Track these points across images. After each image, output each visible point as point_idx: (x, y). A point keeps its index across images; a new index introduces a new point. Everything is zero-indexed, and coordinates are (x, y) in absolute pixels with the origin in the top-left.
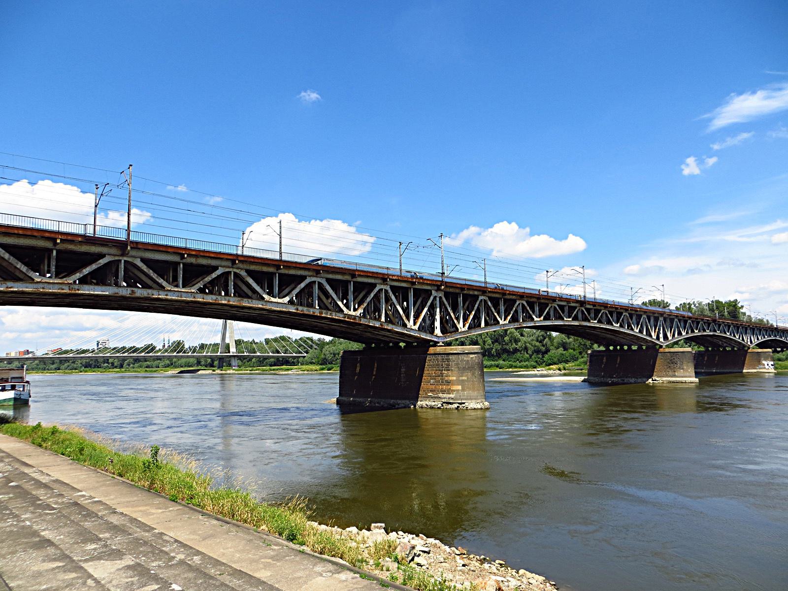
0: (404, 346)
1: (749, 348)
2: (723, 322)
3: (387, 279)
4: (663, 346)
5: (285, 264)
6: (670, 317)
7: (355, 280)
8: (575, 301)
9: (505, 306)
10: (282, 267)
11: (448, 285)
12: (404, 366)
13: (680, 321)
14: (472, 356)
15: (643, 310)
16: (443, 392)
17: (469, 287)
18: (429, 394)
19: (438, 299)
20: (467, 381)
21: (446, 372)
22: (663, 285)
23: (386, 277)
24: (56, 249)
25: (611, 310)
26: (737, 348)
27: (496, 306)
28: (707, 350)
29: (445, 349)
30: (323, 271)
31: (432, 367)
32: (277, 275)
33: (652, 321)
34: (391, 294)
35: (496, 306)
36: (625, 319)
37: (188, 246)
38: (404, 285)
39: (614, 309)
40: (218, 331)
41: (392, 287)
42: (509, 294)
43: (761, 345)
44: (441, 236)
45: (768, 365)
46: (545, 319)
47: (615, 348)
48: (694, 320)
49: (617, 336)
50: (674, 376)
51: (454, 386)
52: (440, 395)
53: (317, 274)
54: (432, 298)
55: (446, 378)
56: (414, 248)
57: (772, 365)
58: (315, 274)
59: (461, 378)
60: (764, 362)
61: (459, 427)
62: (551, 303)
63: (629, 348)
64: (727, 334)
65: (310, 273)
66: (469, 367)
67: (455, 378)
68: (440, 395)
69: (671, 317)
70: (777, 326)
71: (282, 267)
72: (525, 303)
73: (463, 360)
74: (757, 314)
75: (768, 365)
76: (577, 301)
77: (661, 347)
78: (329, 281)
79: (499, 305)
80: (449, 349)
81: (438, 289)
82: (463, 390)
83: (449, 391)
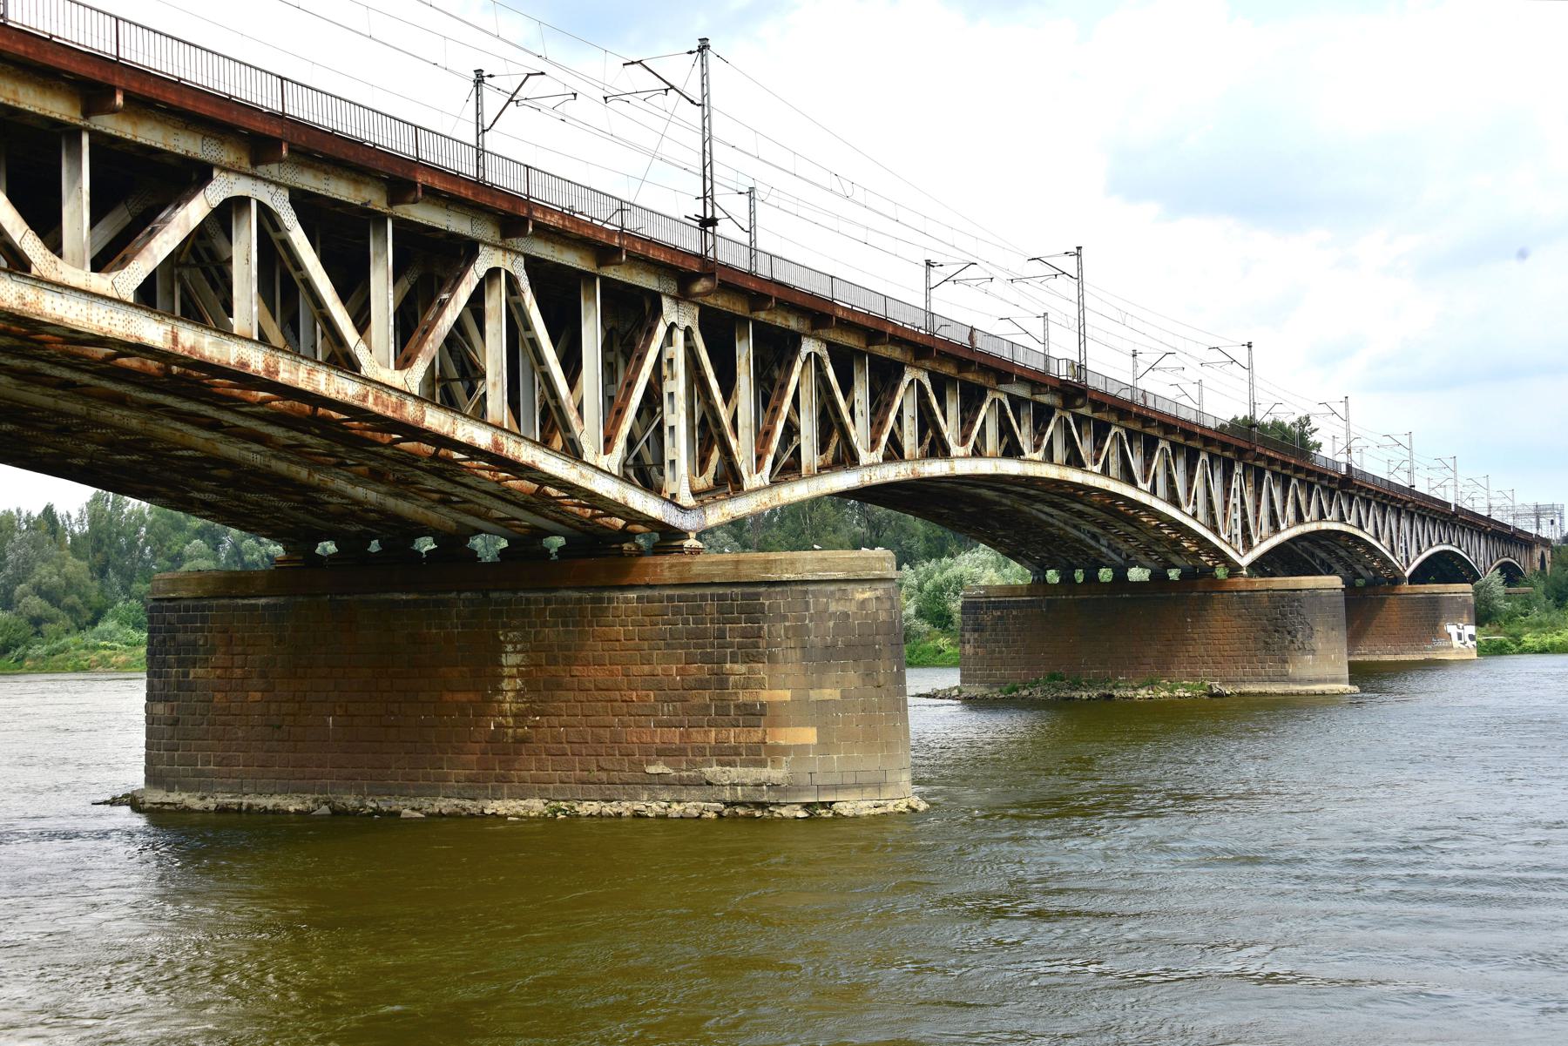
3: (525, 221)
5: (135, 87)
9: (406, 285)
10: (119, 100)
11: (733, 282)
12: (515, 644)
13: (844, 361)
16: (726, 755)
18: (652, 770)
19: (679, 336)
20: (843, 704)
21: (740, 668)
22: (1249, 346)
23: (524, 212)
28: (1040, 581)
29: (737, 562)
31: (668, 646)
33: (744, 353)
36: (496, 304)
47: (1067, 579)
50: (1284, 678)
52: (712, 771)
53: (255, 163)
55: (743, 696)
57: (1472, 637)
59: (815, 695)
60: (1452, 629)
63: (1120, 575)
64: (1141, 485)
66: (848, 646)
67: (786, 695)
68: (712, 771)
70: (1349, 467)
71: (119, 100)
73: (822, 615)
78: (303, 203)
80: (753, 564)
81: (683, 296)
82: (825, 745)
83: (757, 755)
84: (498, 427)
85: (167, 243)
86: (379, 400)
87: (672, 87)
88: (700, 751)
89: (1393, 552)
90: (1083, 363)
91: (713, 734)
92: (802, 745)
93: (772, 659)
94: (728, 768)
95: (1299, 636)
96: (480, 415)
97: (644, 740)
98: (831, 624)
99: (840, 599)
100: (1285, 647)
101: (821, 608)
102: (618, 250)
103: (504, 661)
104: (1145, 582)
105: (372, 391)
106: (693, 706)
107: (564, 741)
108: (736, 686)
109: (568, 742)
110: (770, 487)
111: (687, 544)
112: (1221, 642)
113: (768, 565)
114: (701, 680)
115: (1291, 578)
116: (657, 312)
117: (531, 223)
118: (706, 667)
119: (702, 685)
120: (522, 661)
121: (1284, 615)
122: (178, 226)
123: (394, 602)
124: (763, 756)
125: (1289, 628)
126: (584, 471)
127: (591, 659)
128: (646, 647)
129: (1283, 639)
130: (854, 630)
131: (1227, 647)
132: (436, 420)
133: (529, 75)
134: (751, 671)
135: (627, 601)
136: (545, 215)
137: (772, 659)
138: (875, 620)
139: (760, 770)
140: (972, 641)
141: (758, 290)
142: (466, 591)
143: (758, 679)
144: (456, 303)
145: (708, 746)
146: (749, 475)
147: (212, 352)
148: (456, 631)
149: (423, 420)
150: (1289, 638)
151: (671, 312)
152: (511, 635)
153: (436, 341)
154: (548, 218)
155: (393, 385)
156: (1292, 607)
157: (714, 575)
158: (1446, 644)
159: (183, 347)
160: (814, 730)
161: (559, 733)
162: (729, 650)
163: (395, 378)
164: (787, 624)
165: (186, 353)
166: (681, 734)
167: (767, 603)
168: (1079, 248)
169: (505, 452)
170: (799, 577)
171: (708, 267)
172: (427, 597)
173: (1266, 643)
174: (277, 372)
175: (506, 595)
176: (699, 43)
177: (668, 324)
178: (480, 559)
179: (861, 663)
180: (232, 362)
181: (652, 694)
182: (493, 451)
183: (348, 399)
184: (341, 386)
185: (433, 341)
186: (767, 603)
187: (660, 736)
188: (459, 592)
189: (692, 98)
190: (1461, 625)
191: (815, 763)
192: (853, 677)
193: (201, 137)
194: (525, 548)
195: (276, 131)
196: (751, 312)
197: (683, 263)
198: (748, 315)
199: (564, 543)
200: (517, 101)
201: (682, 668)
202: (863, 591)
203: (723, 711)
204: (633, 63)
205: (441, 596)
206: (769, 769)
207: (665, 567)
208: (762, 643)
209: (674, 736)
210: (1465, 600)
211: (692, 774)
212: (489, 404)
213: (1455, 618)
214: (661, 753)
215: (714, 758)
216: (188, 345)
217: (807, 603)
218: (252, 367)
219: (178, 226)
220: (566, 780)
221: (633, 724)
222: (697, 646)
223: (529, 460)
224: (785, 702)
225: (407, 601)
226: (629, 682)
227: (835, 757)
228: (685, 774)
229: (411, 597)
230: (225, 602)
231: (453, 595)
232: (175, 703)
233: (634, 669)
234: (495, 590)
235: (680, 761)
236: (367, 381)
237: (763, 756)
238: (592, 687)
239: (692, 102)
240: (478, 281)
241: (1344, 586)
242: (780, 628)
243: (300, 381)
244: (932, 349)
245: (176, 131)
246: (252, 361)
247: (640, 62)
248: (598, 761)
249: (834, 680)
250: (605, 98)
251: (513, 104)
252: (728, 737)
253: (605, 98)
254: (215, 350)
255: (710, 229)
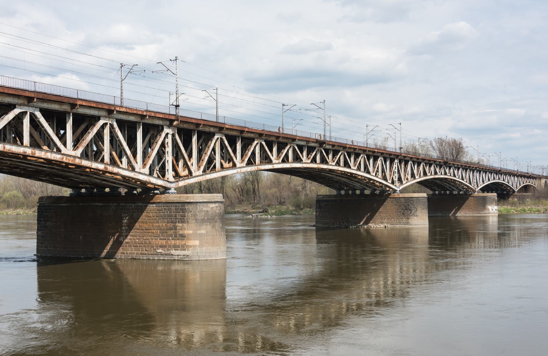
0: (126, 193)
1: (474, 191)
2: (454, 164)
3: (113, 111)
4: (397, 191)
6: (430, 162)
7: (74, 111)
8: (315, 141)
11: (185, 121)
14: (213, 205)
15: (380, 151)
16: (176, 247)
17: (206, 123)
18: (158, 251)
21: (180, 225)
23: (113, 108)
24: (197, 130)
25: (349, 150)
26: (86, 188)
27: (233, 145)
29: (180, 197)
30: (37, 98)
31: (163, 219)
32: (141, 123)
34: (117, 130)
35: (233, 145)
36: (107, 131)
37: (337, 141)
38: (132, 118)
39: (352, 150)
40: (25, 181)
41: (119, 122)
42: (248, 132)
43: (487, 189)
44: (176, 59)
45: (492, 210)
46: (283, 161)
48: (427, 162)
49: (352, 180)
51: (190, 241)
53: (29, 102)
54: (163, 135)
55: (181, 232)
56: (140, 72)
58: (26, 103)
59: (198, 232)
61: (295, 269)
62: (291, 143)
65: (20, 101)
67: (191, 232)
69: (406, 159)
72: (264, 143)
73: (201, 211)
74: (482, 154)
75: (492, 210)
76: (317, 141)
77: (395, 191)
79: (420, 165)
80: (184, 198)
81: (170, 125)
82: (201, 245)
83: (184, 247)
84: (107, 164)
85: (2, 124)
86: (67, 159)
87: (169, 70)
88: (170, 246)
89: (470, 183)
90: (325, 134)
91: (173, 242)
92: (195, 245)
93: (188, 222)
94: (177, 251)
95: (413, 211)
96: (102, 161)
97: (157, 243)
98: (203, 213)
99: (206, 207)
100: (409, 214)
101: (201, 209)
102: (146, 116)
103: (123, 222)
104: (369, 194)
105: (65, 157)
106: (169, 234)
107: (137, 243)
108: (179, 230)
109: (138, 243)
110: (202, 175)
111: (170, 191)
112: (390, 213)
113: (187, 198)
114: (171, 228)
115: (410, 194)
116: (163, 129)
117: (115, 111)
118: (172, 224)
119: (171, 229)
120: (127, 222)
121: (408, 205)
122: (5, 120)
123: (96, 205)
124: (185, 248)
125: (411, 209)
126: (135, 174)
127: (144, 222)
128: (157, 219)
129: (408, 212)
130: (209, 215)
131: (392, 214)
132: (85, 163)
133: (134, 65)
134: (183, 225)
135: (153, 207)
136: (120, 109)
137: (188, 222)
138: (215, 212)
139: (184, 251)
140: (318, 211)
141: (196, 122)
142: (115, 203)
143: (184, 228)
144: (93, 133)
145: (172, 245)
146: (195, 172)
147: (15, 150)
148: (112, 213)
149: (81, 163)
150: (410, 212)
151: (166, 130)
152: (125, 215)
153: (86, 143)
154: (121, 109)
155: (72, 155)
156: (411, 202)
157: (174, 200)
158: (488, 212)
159: (7, 149)
160: (198, 241)
161: (136, 241)
162: (177, 220)
163: (73, 153)
164: (192, 213)
165: (7, 151)
166: (166, 242)
167: (187, 208)
168: (324, 101)
169: (108, 170)
170: (195, 201)
171: (177, 118)
172: (105, 204)
173: (403, 213)
174: (35, 154)
175: (124, 204)
176: (175, 58)
177: (166, 133)
178: (122, 194)
179: (211, 224)
180: (21, 152)
181: (159, 231)
182: (104, 170)
183: (57, 159)
184: (55, 156)
185: (85, 143)
186: (187, 208)
187: (160, 242)
188: (113, 203)
189: (173, 73)
190: (493, 206)
191: (198, 250)
192: (209, 227)
193: (12, 98)
194: (129, 194)
195: (32, 95)
196: (196, 128)
197: (168, 117)
198: (195, 128)
199: (141, 190)
200: (131, 72)
201: (166, 224)
202: (212, 205)
203: (176, 236)
204: (159, 63)
205: (108, 204)
206: (186, 251)
207: (163, 198)
208: (185, 218)
209: (164, 242)
210: (494, 198)
211: (168, 252)
212: (105, 158)
213: (491, 203)
214: (161, 247)
215: (173, 248)
216: (8, 149)
217: (197, 208)
218: (28, 153)
219: (5, 120)
220: (138, 253)
221: (154, 239)
222: (170, 219)
223: (117, 172)
224: (191, 234)
225: (100, 206)
226: (153, 228)
227: (204, 248)
228: (166, 252)
229: (101, 204)
230: (56, 205)
231: (112, 204)
232: (43, 231)
233: (155, 225)
234: (121, 203)
235: (165, 249)
236: (64, 154)
237: (185, 248)
238: (144, 229)
239: (174, 74)
240: (100, 126)
241: (427, 196)
242: (190, 214)
243: (42, 155)
244: (263, 134)
245: (5, 97)
246: (28, 152)
247: (161, 63)
248: (145, 249)
249: (204, 228)
250: (152, 72)
251: (130, 73)
252: (177, 243)
253: (152, 72)
254: (16, 149)
255: (178, 107)
